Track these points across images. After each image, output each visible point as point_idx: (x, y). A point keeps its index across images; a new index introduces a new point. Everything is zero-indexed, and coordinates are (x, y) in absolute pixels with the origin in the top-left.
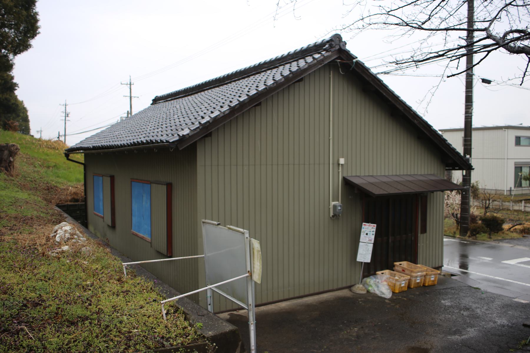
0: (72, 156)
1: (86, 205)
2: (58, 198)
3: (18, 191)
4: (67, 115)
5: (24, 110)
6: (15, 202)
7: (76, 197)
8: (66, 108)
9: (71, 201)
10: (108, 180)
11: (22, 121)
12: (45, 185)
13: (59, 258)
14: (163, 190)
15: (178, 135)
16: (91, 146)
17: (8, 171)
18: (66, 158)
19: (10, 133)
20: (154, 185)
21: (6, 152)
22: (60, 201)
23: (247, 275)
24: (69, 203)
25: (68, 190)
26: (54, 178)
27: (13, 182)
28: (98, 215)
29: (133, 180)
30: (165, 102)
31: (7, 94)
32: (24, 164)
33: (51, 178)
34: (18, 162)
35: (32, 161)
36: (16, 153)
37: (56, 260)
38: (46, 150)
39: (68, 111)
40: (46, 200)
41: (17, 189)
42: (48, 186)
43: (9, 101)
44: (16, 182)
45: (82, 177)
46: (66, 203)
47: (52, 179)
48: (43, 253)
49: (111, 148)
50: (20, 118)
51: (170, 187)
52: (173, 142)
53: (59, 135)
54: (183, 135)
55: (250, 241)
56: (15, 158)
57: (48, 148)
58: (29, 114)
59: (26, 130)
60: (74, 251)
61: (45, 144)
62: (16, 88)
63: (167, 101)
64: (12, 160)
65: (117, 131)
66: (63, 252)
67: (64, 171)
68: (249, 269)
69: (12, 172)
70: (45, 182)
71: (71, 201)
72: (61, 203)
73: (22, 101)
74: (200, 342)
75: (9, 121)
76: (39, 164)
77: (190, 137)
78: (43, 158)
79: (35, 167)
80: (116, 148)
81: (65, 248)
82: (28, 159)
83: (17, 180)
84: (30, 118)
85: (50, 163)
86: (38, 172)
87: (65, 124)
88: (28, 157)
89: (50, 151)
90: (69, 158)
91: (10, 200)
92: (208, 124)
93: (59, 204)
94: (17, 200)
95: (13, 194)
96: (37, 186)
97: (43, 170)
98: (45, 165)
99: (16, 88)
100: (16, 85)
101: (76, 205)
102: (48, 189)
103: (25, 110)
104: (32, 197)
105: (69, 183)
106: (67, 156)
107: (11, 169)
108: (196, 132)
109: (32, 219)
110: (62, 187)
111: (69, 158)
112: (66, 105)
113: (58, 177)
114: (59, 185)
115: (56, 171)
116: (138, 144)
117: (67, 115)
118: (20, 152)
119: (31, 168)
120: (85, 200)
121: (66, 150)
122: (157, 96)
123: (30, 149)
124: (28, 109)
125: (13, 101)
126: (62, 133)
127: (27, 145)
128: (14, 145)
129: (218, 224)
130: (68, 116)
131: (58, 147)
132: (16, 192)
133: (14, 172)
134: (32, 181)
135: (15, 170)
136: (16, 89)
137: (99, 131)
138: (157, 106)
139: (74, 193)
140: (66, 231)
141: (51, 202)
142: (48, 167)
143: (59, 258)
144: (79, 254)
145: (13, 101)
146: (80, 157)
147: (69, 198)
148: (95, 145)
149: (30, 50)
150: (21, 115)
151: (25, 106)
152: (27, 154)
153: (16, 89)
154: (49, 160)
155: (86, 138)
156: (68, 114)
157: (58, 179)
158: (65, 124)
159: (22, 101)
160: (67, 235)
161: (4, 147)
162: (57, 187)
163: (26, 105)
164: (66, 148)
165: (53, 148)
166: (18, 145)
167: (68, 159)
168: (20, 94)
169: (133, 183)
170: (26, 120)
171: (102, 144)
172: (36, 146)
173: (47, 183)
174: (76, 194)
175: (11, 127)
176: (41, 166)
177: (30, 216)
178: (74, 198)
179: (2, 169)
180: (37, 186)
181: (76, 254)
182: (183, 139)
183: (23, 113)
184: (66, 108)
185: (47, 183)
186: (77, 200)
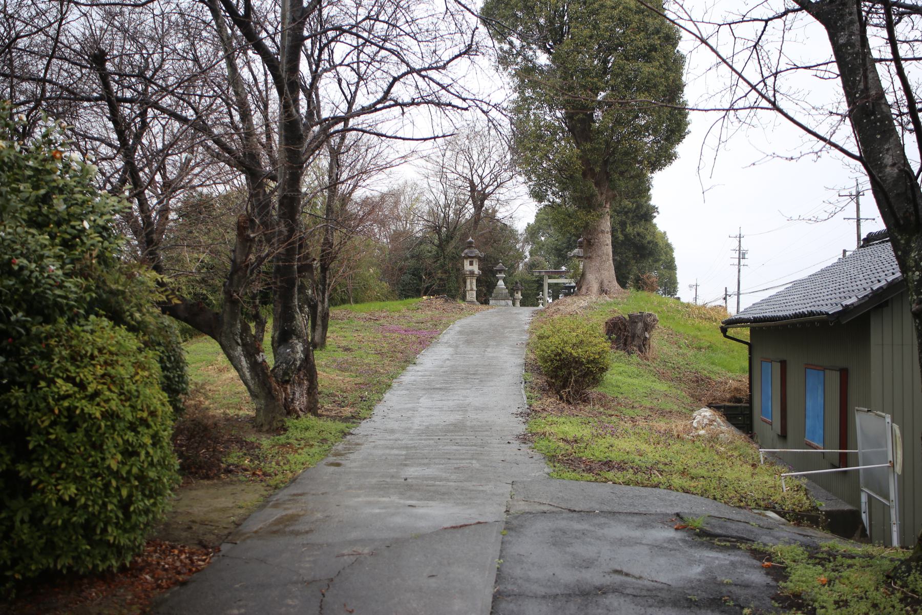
0: (731, 332)
1: (751, 408)
2: (711, 395)
3: (655, 381)
4: (742, 255)
5: (668, 249)
6: (650, 394)
7: (738, 396)
8: (740, 241)
9: (729, 401)
10: (777, 366)
11: (664, 268)
12: (693, 375)
13: (694, 441)
14: (834, 378)
15: (842, 305)
16: (751, 317)
17: (642, 352)
18: (722, 334)
19: (643, 294)
20: (827, 371)
21: (640, 325)
22: (714, 399)
23: (888, 465)
24: (727, 404)
25: (726, 383)
26: (706, 366)
27: (648, 368)
28: (766, 422)
29: (808, 366)
30: (880, 243)
31: (640, 227)
32: (663, 342)
33: (702, 365)
34: (656, 340)
35: (675, 339)
36: (653, 327)
37: (691, 442)
38: (697, 321)
39: (743, 247)
40: (692, 396)
41: (654, 379)
42: (696, 377)
43: (644, 238)
44: (652, 368)
45: (746, 364)
46: (723, 404)
47: (703, 366)
48: (678, 435)
49: (774, 321)
50: (661, 262)
51: (844, 374)
52: (833, 314)
53: (726, 295)
54: (846, 305)
55: (892, 427)
56: (652, 333)
57: (701, 318)
58: (675, 255)
59: (670, 286)
60: (710, 435)
61: (697, 311)
62: (655, 214)
63: (883, 242)
64: (648, 336)
65: (334, 418)
66: (699, 436)
67: (723, 355)
68: (890, 458)
69: (647, 354)
70: (694, 371)
71: (729, 401)
72: (715, 403)
73: (665, 233)
74: (813, 513)
75: (642, 274)
76: (685, 343)
77: (855, 307)
78: (692, 334)
79: (680, 347)
80: (819, 315)
81: (702, 432)
82: (670, 336)
83: (655, 365)
84: (677, 262)
85: (702, 342)
86: (683, 355)
87: (739, 271)
88: (670, 332)
89: (704, 322)
90: (728, 334)
91: (644, 391)
92: (881, 291)
93: (711, 403)
94: (653, 392)
95: (649, 384)
96: (682, 375)
97: (690, 353)
98: (694, 346)
99: (655, 214)
100: (654, 209)
101: (737, 407)
102: (697, 381)
103: (669, 248)
104: (674, 390)
105: (730, 374)
106: (724, 330)
107: (646, 349)
108: (863, 301)
109: (670, 412)
110: (719, 380)
111: (728, 334)
112: (740, 237)
113: (713, 364)
114: (713, 376)
115: (711, 354)
116: (802, 315)
117: (742, 255)
118: (659, 325)
119: (674, 349)
120: (750, 400)
121: (723, 323)
122: (870, 233)
123: (674, 319)
124: (673, 246)
125: (649, 238)
126: (733, 289)
127: (669, 314)
128: (650, 315)
129: (868, 411)
130: (744, 258)
131: (717, 317)
132: (652, 382)
133: (649, 355)
134: (674, 368)
135: (651, 351)
136: (655, 217)
137: (773, 292)
138: (868, 250)
139: (735, 388)
140: (704, 416)
141: (700, 400)
142: (700, 349)
143: (694, 441)
144: (716, 440)
145: (649, 238)
146: (745, 333)
147: (728, 396)
148: (756, 316)
149: (676, 163)
150: (663, 258)
151: (669, 242)
152: (669, 327)
153: (655, 217)
154: (701, 338)
155: (754, 304)
156: (744, 254)
157: (712, 366)
158: (739, 271)
159: (665, 233)
160: (706, 421)
161: (637, 317)
162: (710, 379)
163: (671, 239)
164: (728, 318)
165: (709, 319)
166: (656, 315)
167: (726, 336)
168: (660, 222)
169: (808, 370)
170: (671, 266)
171: (764, 315)
172: (682, 315)
173: (697, 372)
174: (737, 390)
175: (645, 283)
176: (688, 346)
177: (668, 410)
178: (734, 397)
179: (635, 348)
180: (682, 375)
181: (713, 439)
182: (847, 310)
183: (666, 253)
184: (740, 241)
185: (697, 372)
186: (739, 400)
